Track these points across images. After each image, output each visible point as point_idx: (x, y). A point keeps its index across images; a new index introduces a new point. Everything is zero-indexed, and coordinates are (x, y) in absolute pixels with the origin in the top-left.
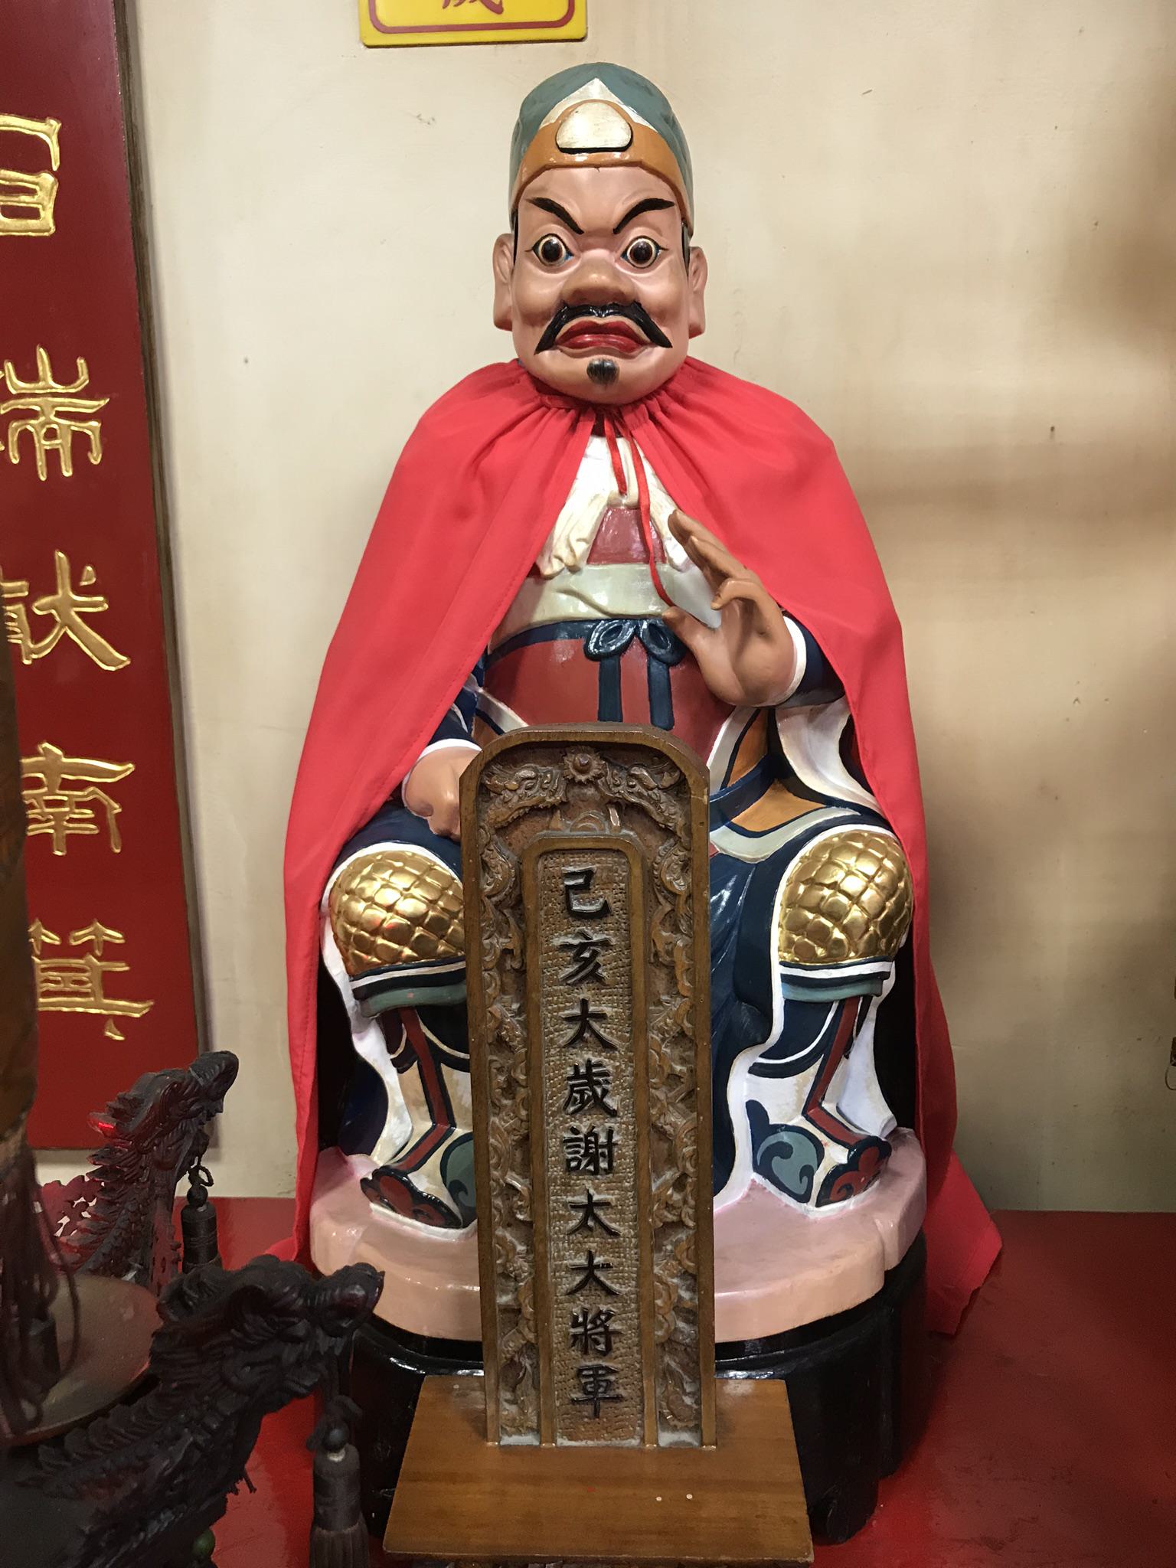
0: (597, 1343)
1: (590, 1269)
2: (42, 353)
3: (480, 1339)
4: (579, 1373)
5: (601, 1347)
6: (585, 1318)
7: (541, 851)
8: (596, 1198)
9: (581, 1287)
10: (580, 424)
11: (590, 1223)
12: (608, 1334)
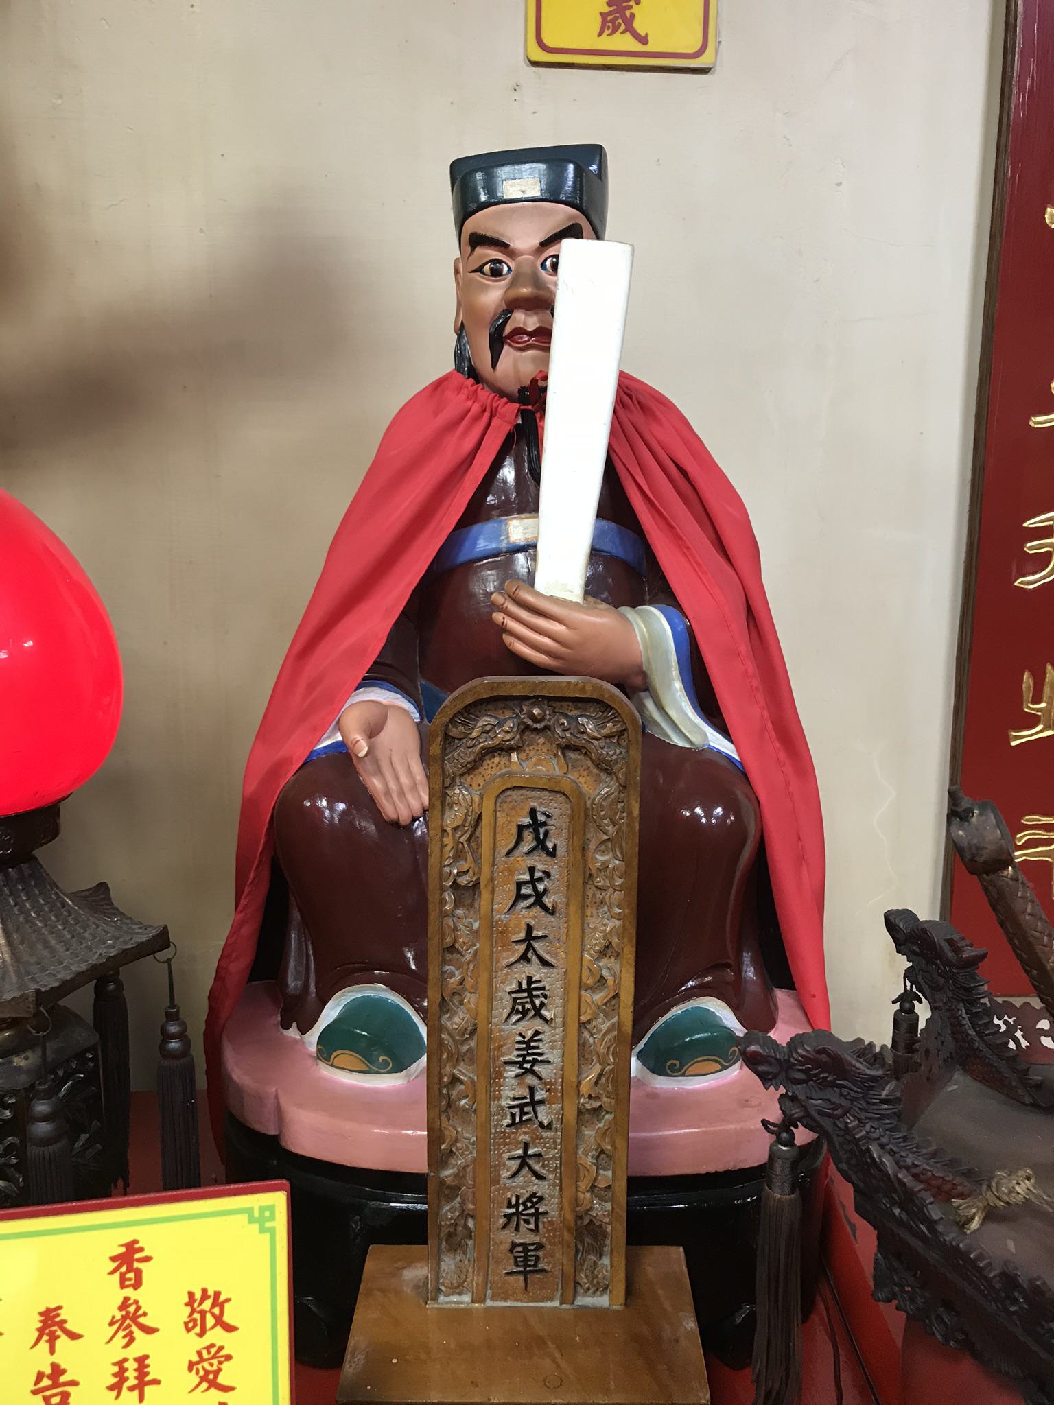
4: (514, 1245)
10: (536, 853)
12: (537, 1215)
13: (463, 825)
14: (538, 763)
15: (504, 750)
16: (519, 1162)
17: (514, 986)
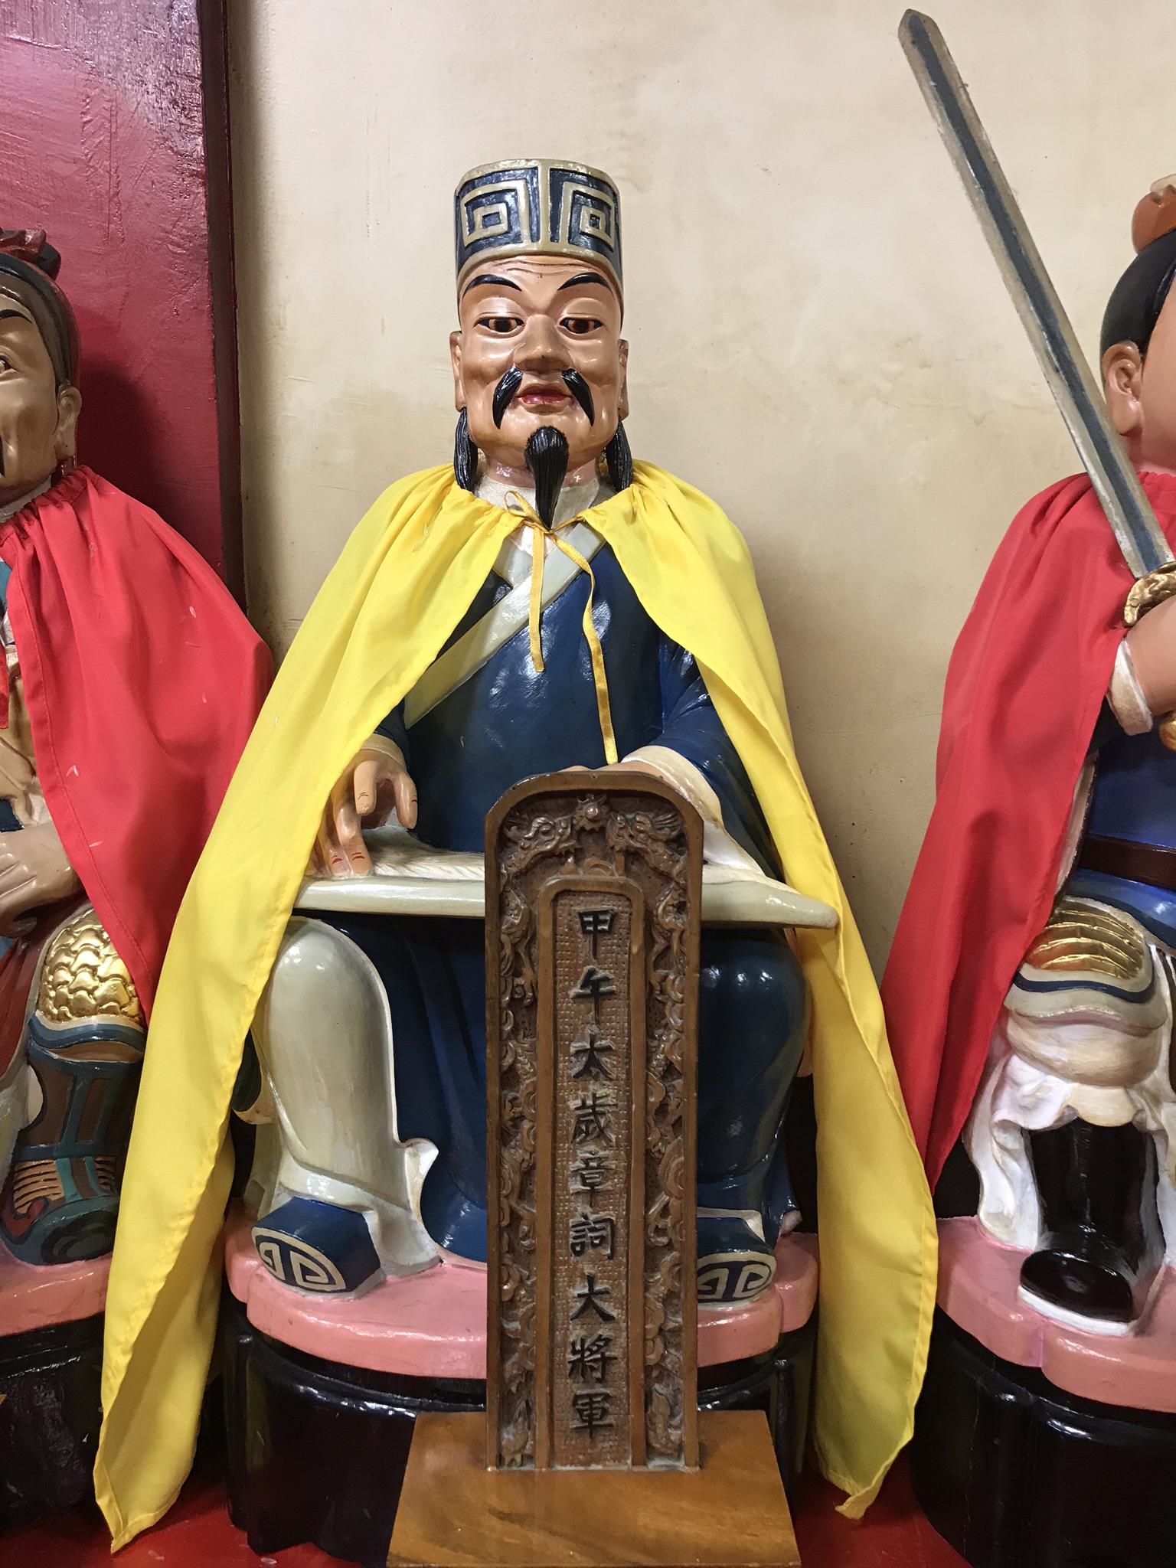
0: (592, 1369)
3: (483, 1375)
5: (599, 1375)
6: (582, 1345)
9: (582, 1310)
12: (606, 1361)
13: (528, 948)
14: (599, 872)
15: (554, 858)
16: (583, 1300)
17: (579, 1102)
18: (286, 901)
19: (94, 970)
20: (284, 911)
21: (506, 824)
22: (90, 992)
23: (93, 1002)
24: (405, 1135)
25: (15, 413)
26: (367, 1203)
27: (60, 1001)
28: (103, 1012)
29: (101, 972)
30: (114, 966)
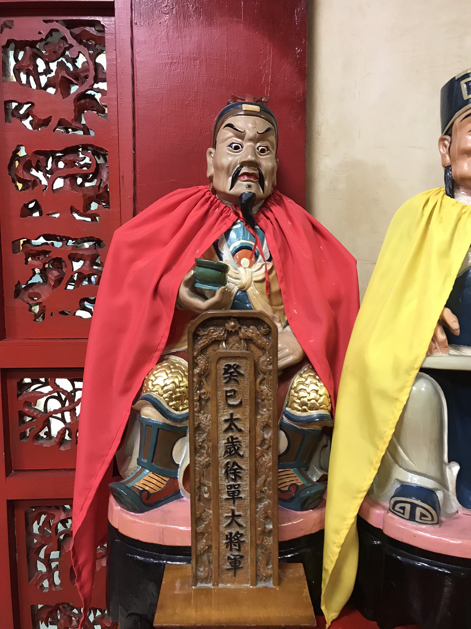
1: (234, 515)
2: (51, 158)
3: (190, 544)
7: (216, 359)
8: (237, 513)
11: (233, 427)
14: (234, 347)
18: (418, 365)
19: (317, 391)
20: (417, 369)
21: (197, 329)
22: (317, 401)
23: (318, 405)
24: (450, 461)
25: (270, 168)
26: (439, 488)
27: (303, 404)
28: (322, 409)
29: (320, 392)
30: (323, 390)
